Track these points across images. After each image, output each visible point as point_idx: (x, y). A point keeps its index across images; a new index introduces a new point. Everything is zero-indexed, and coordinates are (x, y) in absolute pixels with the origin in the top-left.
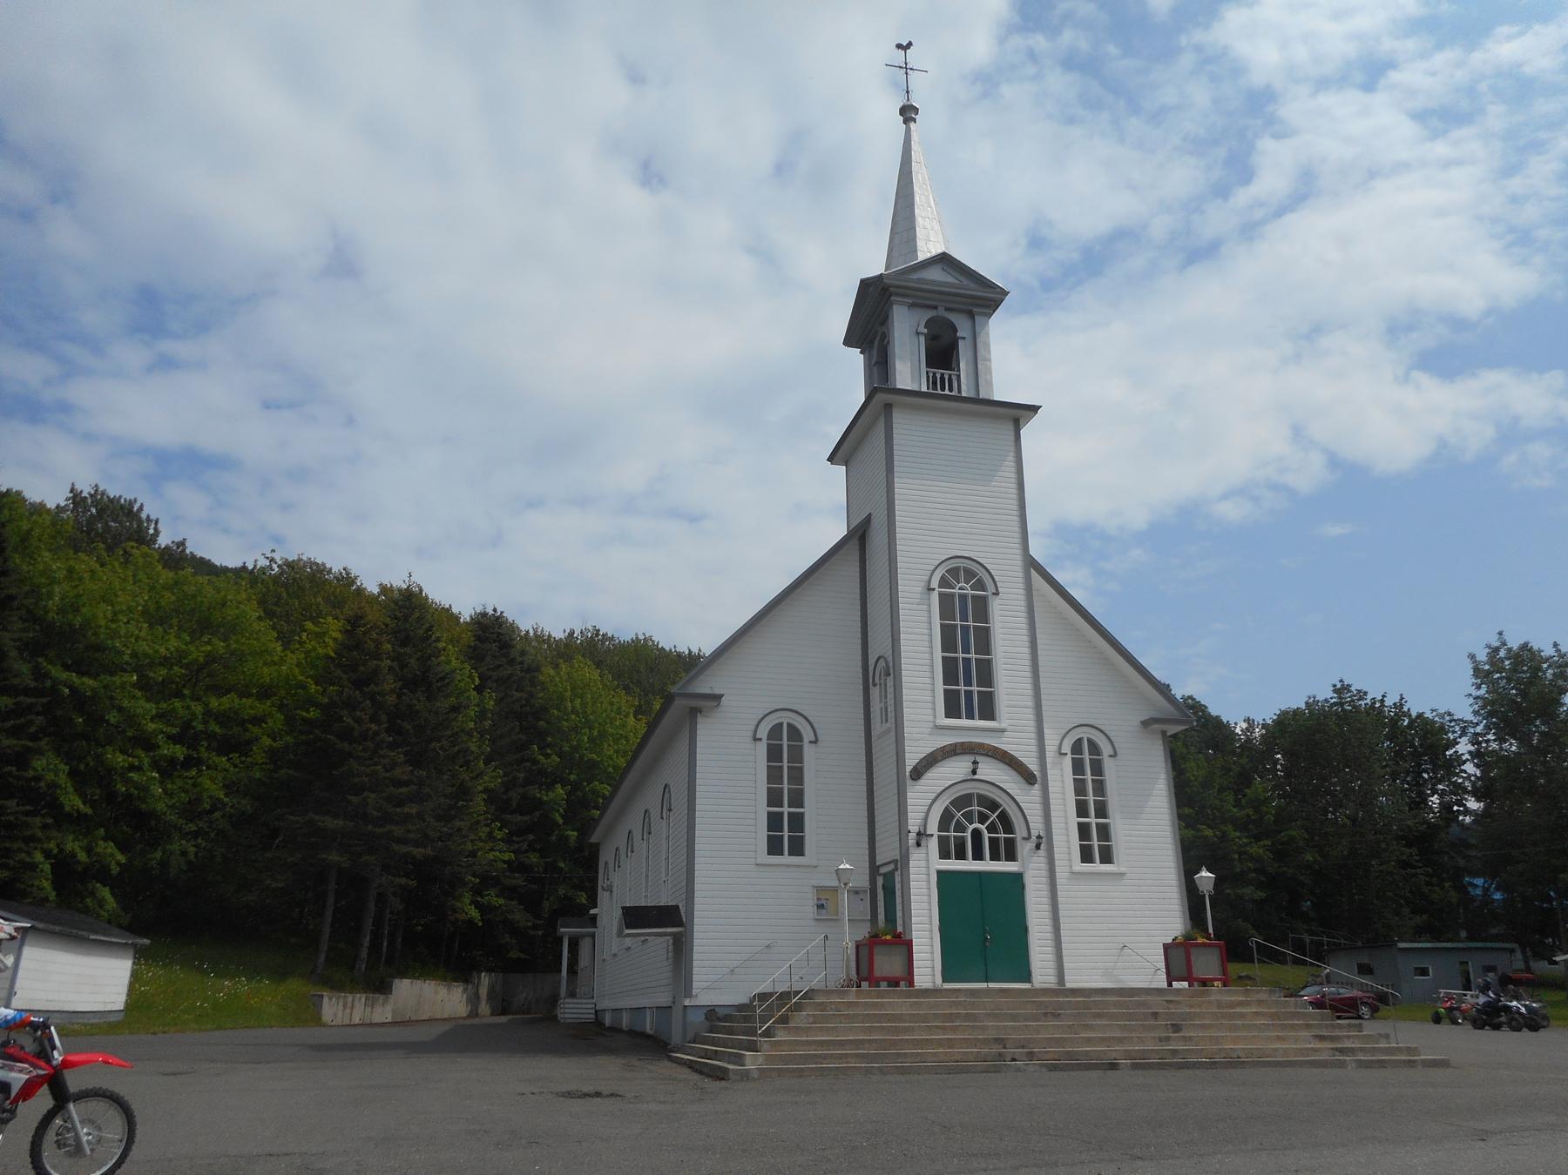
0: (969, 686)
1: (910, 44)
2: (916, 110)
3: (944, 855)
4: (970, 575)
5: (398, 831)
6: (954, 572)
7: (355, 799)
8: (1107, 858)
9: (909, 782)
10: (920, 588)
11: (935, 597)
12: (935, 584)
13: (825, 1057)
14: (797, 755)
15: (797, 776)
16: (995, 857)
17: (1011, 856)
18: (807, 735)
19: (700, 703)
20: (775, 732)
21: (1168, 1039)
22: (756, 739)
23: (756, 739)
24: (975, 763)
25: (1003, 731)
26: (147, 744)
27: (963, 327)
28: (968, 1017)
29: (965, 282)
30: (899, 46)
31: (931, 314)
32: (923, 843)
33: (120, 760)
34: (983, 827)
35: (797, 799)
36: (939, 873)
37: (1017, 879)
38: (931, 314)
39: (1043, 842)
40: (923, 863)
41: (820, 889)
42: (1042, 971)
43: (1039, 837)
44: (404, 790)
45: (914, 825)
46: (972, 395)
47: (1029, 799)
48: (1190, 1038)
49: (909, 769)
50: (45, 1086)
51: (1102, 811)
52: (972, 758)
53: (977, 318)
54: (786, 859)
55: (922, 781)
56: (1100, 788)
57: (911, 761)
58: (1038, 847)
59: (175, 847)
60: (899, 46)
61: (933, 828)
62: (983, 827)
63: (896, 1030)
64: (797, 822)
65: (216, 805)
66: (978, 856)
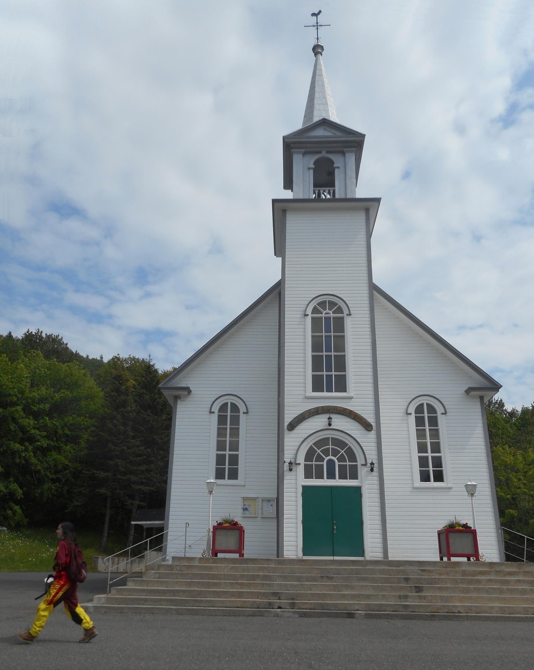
0: (330, 370)
1: (320, 12)
2: (322, 48)
3: (308, 475)
4: (332, 304)
5: (133, 478)
6: (322, 304)
7: (111, 462)
8: (439, 477)
9: (286, 432)
10: (299, 314)
11: (309, 320)
12: (309, 311)
13: (146, 600)
14: (236, 420)
15: (235, 432)
16: (343, 477)
17: (354, 476)
18: (242, 409)
19: (177, 393)
20: (223, 408)
21: (406, 597)
22: (211, 412)
23: (211, 412)
24: (330, 418)
25: (351, 398)
26: (32, 440)
27: (337, 160)
28: (265, 577)
29: (338, 134)
30: (313, 15)
31: (316, 157)
32: (294, 469)
33: (17, 446)
34: (335, 459)
35: (235, 446)
36: (304, 487)
37: (358, 490)
38: (316, 157)
39: (376, 467)
40: (293, 481)
41: (245, 499)
42: (372, 548)
43: (372, 464)
44: (139, 458)
45: (288, 457)
46: (343, 197)
47: (367, 440)
48: (425, 597)
49: (286, 424)
50: (63, 602)
51: (436, 448)
52: (328, 416)
53: (347, 155)
54: (226, 481)
55: (295, 431)
56: (435, 434)
57: (288, 418)
58: (372, 470)
59: (46, 486)
60: (313, 15)
61: (301, 459)
62: (335, 459)
63: (208, 585)
64: (234, 460)
65: (66, 468)
66: (331, 476)
